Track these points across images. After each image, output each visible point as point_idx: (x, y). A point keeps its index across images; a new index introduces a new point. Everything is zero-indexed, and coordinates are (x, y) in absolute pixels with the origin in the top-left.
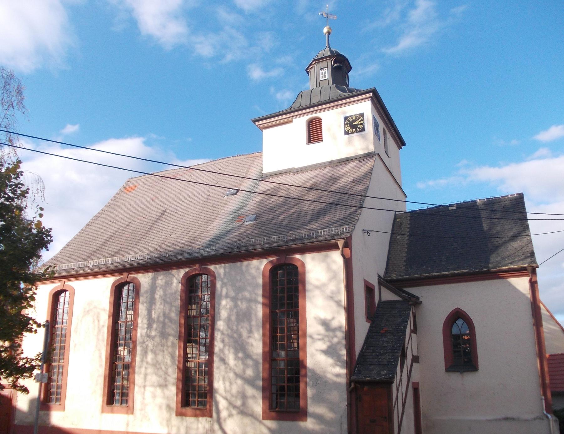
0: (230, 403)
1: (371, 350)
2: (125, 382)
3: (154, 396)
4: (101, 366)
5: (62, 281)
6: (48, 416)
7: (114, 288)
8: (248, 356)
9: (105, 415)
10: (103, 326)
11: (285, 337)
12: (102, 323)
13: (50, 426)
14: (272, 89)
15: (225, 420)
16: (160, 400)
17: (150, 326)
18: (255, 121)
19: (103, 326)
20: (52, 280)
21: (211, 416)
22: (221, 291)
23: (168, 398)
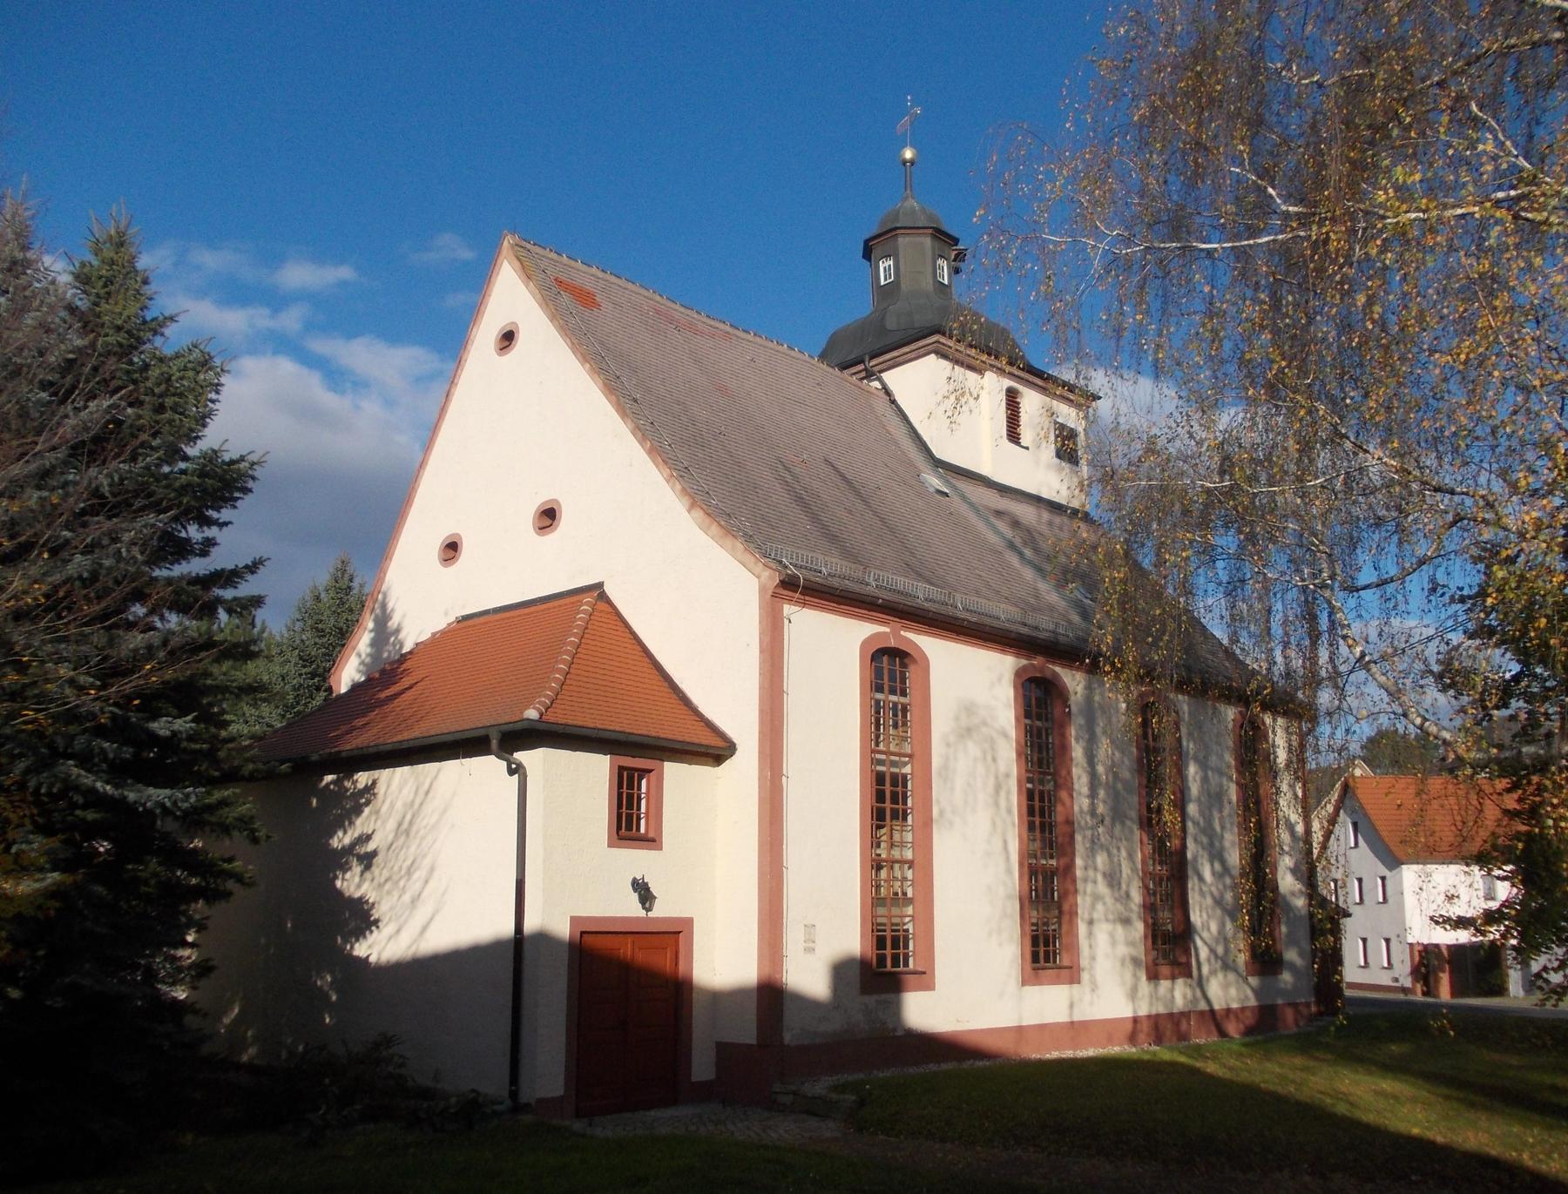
0: (1212, 951)
1: (1395, 15)
2: (1117, 895)
3: (1114, 943)
4: (1009, 871)
5: (897, 623)
6: (896, 1009)
7: (1019, 686)
8: (1226, 869)
9: (1027, 988)
10: (1007, 776)
11: (885, 959)
12: (1002, 768)
13: (899, 1033)
14: (1310, 726)
15: (1208, 980)
16: (1123, 950)
17: (1093, 795)
18: (1364, 940)
19: (1007, 776)
20: (869, 611)
21: (1189, 975)
22: (1188, 746)
23: (1131, 943)
